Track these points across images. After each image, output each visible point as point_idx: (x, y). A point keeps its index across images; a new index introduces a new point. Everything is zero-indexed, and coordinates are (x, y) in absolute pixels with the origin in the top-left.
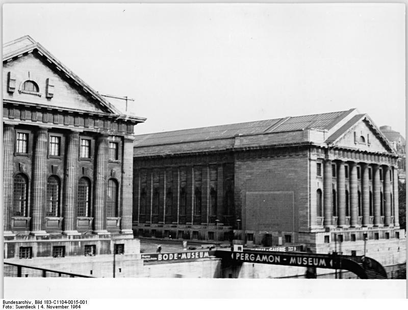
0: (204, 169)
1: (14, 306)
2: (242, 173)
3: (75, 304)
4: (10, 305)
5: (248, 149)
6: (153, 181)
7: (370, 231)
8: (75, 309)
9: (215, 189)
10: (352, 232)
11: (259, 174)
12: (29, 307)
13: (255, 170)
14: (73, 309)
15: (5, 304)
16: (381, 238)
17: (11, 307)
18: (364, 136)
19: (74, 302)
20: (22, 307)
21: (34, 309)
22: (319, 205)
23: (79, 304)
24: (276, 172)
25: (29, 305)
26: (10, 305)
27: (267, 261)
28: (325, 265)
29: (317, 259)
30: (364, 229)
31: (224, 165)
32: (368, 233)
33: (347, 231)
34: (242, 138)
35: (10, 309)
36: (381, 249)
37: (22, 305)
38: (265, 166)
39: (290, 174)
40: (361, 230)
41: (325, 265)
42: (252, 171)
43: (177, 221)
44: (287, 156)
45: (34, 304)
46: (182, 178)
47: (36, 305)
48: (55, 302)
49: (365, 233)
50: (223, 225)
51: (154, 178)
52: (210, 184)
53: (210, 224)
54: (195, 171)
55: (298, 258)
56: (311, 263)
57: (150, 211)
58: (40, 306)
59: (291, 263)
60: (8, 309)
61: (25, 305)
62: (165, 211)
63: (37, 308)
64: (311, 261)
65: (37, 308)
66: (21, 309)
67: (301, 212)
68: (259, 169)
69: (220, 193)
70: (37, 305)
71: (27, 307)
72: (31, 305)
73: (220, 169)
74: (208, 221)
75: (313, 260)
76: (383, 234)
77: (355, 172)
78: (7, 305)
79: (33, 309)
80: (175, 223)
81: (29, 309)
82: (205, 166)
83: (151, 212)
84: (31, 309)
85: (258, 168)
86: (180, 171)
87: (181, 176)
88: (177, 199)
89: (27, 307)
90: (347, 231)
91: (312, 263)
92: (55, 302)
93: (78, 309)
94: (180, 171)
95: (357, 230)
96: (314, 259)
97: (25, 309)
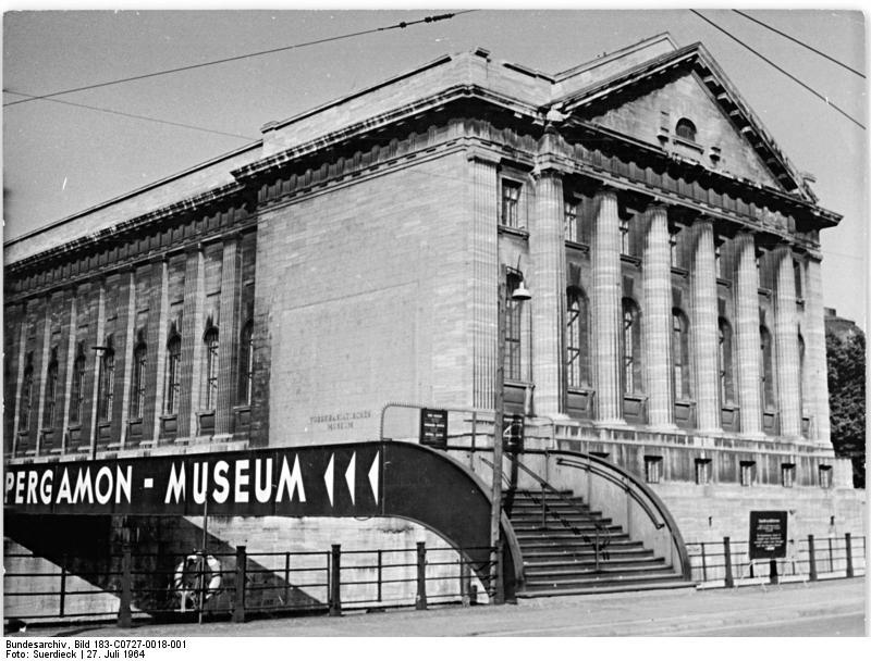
0: (191, 262)
1: (30, 652)
2: (276, 250)
3: (134, 650)
4: (21, 650)
6: (77, 322)
7: (722, 453)
8: (133, 659)
9: (215, 324)
10: (647, 448)
11: (320, 243)
12: (63, 655)
13: (308, 233)
14: (128, 659)
15: (11, 648)
17: (23, 655)
19: (157, 644)
20: (46, 655)
21: (74, 659)
23: (142, 648)
24: (366, 227)
25: (62, 650)
26: (21, 650)
28: (302, 498)
31: (237, 238)
32: (715, 457)
33: (630, 442)
34: (534, 311)
35: (21, 659)
37: (47, 650)
38: (338, 209)
39: (407, 225)
40: (687, 445)
41: (302, 498)
42: (302, 236)
43: (119, 441)
45: (73, 647)
46: (140, 300)
47: (78, 651)
48: (117, 644)
50: (228, 440)
51: (78, 313)
52: (203, 309)
53: (198, 439)
54: (170, 274)
56: (243, 488)
57: (62, 415)
58: (86, 654)
60: (17, 659)
61: (54, 650)
62: (94, 410)
63: (79, 657)
64: (245, 480)
65: (79, 657)
66: (44, 659)
67: (440, 358)
68: (319, 226)
69: (227, 331)
70: (80, 650)
71: (57, 654)
72: (65, 650)
73: (230, 252)
74: (193, 431)
75: (250, 472)
78: (15, 650)
79: (70, 659)
80: (116, 445)
81: (61, 659)
82: (191, 252)
83: (66, 418)
84: (66, 659)
85: (317, 222)
86: (137, 282)
87: (137, 295)
89: (57, 654)
90: (630, 442)
91: (250, 488)
92: (117, 644)
93: (140, 658)
94: (137, 282)
95: (672, 444)
96: (258, 462)
97: (53, 659)
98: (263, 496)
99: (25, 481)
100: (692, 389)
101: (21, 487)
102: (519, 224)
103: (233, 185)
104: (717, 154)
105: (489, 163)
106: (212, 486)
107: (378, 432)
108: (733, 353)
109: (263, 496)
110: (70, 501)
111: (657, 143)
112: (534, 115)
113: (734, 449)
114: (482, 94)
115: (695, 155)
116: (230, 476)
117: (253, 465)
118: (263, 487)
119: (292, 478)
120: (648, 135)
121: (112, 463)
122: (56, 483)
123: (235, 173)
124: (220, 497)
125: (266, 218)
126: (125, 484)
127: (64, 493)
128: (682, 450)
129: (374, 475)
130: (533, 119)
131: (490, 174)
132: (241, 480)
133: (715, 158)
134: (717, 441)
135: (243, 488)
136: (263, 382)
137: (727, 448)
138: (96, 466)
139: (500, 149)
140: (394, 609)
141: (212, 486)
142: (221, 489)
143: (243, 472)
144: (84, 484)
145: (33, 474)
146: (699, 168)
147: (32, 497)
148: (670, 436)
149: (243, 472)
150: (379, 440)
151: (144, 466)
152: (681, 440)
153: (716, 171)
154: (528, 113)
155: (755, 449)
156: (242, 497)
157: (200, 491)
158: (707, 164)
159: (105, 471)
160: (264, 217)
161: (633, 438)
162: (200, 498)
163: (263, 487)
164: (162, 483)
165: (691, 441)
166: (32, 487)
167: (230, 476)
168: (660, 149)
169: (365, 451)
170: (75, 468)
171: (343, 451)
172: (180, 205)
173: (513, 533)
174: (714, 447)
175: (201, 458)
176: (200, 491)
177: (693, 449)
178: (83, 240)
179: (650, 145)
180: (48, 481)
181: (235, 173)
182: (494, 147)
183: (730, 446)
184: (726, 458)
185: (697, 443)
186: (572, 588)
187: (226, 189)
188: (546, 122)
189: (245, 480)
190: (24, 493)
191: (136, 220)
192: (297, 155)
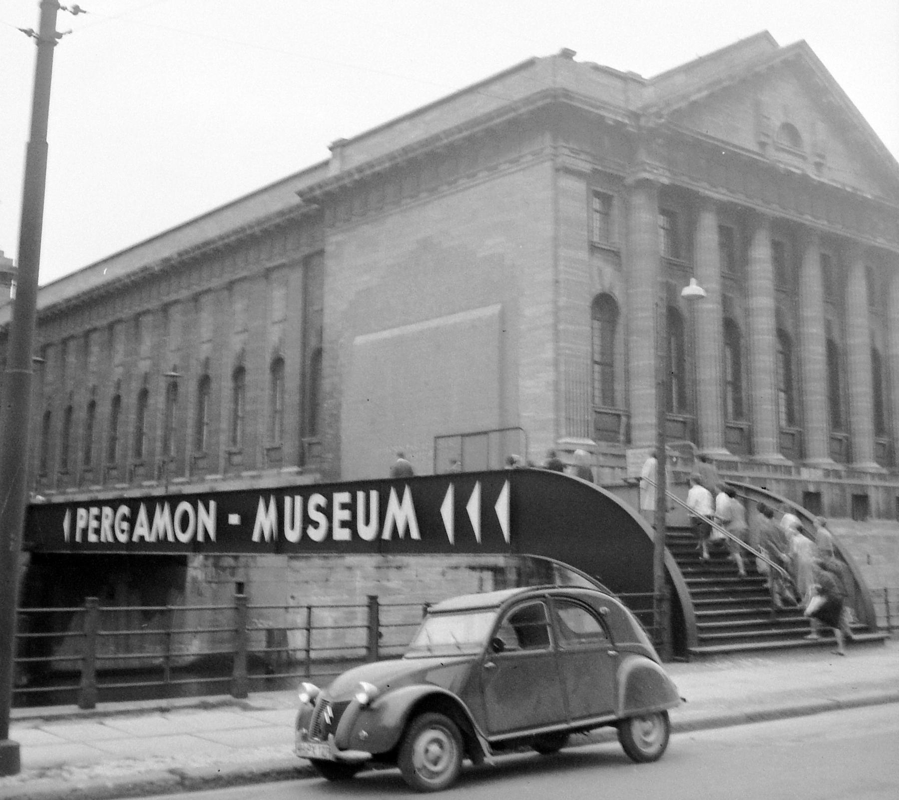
5: (357, 177)
16: (879, 516)
18: (799, 125)
22: (721, 656)
27: (170, 538)
28: (415, 534)
29: (374, 495)
30: (806, 474)
36: (881, 558)
40: (794, 477)
41: (415, 534)
44: (481, 175)
49: (812, 489)
55: (288, 500)
56: (344, 524)
59: (256, 537)
64: (346, 515)
75: (351, 507)
76: (888, 503)
77: (761, 253)
88: (646, 597)
91: (351, 524)
95: (778, 476)
96: (361, 495)
98: (367, 533)
99: (98, 518)
100: (797, 415)
101: (94, 524)
102: (617, 240)
103: (298, 207)
104: (822, 161)
105: (579, 174)
106: (307, 521)
107: (431, 465)
108: (841, 375)
109: (367, 533)
110: (147, 539)
111: (756, 149)
112: (626, 121)
113: (845, 481)
114: (572, 98)
115: (797, 162)
116: (327, 511)
117: (354, 498)
118: (367, 522)
119: (402, 513)
120: (745, 139)
121: (193, 499)
122: (132, 520)
123: (300, 194)
124: (316, 535)
125: (334, 240)
126: (207, 520)
127: (141, 530)
128: (788, 482)
129: (502, 508)
130: (625, 125)
131: (579, 187)
132: (341, 515)
133: (819, 166)
134: (827, 473)
135: (344, 524)
136: (335, 412)
137: (838, 481)
138: (173, 500)
139: (589, 159)
140: (843, 698)
141: (307, 521)
142: (316, 525)
143: (344, 506)
144: (162, 519)
145: (107, 510)
146: (805, 177)
147: (107, 535)
148: (776, 468)
149: (344, 506)
150: (431, 473)
151: (227, 502)
152: (788, 470)
153: (822, 180)
154: (619, 119)
155: (868, 481)
156: (342, 534)
157: (293, 527)
158: (812, 174)
159: (185, 506)
160: (334, 239)
161: (736, 469)
162: (293, 536)
163: (367, 522)
164: (249, 519)
165: (799, 473)
166: (106, 524)
167: (327, 511)
168: (762, 156)
169: (491, 481)
170: (151, 503)
171: (463, 482)
172: (243, 229)
173: (681, 576)
174: (823, 479)
175: (293, 490)
176: (293, 527)
177: (800, 481)
178: (145, 269)
179: (748, 151)
180: (124, 518)
181: (300, 194)
182: (583, 157)
183: (840, 477)
184: (837, 491)
185: (806, 474)
186: (714, 644)
187: (291, 211)
188: (640, 128)
189: (346, 515)
190: (97, 531)
191: (198, 247)
192: (368, 172)
